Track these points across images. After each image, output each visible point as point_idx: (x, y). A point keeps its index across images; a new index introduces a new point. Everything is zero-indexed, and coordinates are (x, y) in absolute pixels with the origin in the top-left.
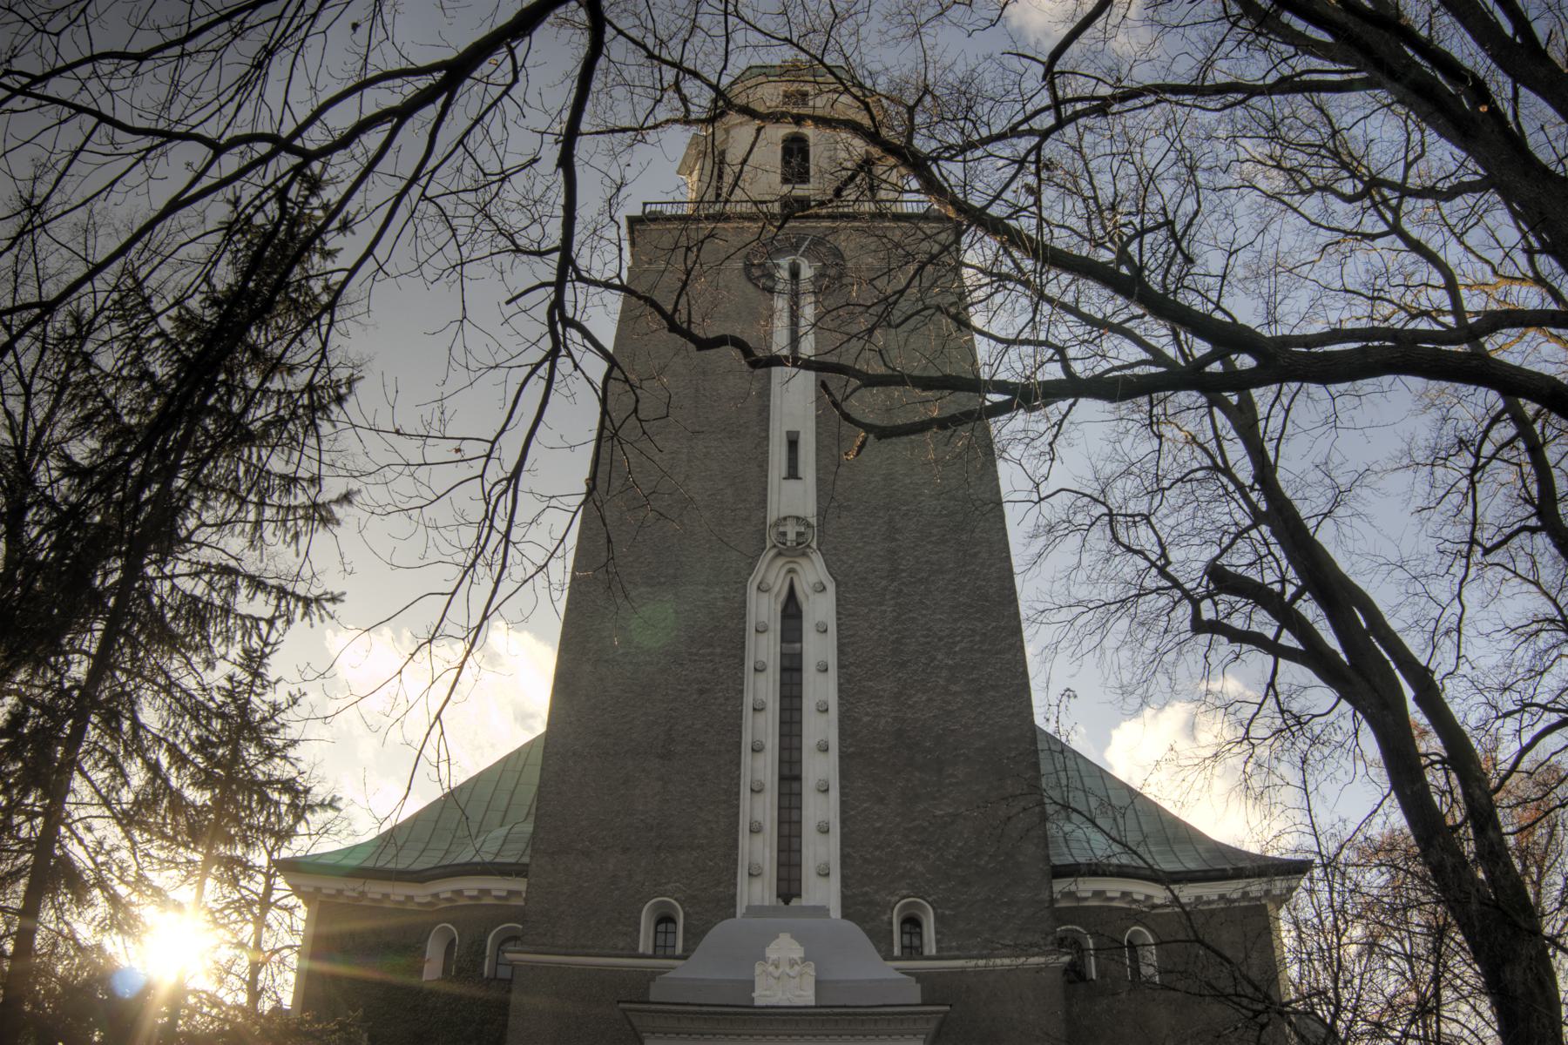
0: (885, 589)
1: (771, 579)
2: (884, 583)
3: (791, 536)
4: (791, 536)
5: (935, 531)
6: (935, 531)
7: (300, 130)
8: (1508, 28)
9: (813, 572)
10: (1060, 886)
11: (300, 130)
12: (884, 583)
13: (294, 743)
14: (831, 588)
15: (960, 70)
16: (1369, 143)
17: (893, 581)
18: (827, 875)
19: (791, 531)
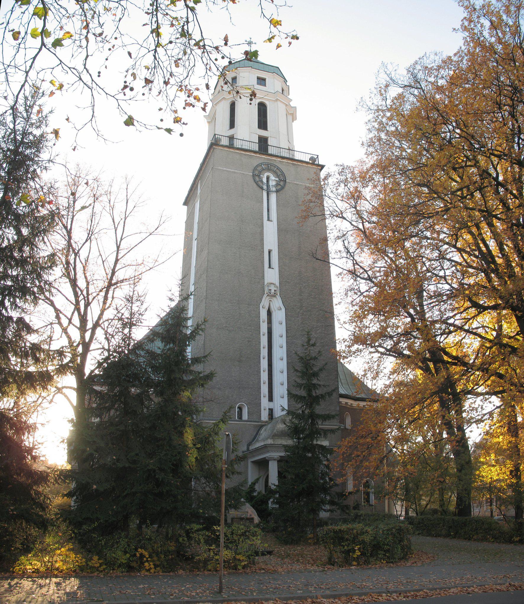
0: (299, 312)
1: (265, 304)
2: (298, 310)
3: (273, 291)
4: (273, 291)
5: (313, 294)
6: (313, 294)
7: (54, 288)
8: (484, 249)
9: (277, 303)
10: (341, 400)
11: (54, 288)
12: (298, 310)
13: (130, 296)
14: (283, 310)
15: (321, 403)
16: (469, 438)
17: (301, 310)
18: (282, 360)
19: (273, 288)
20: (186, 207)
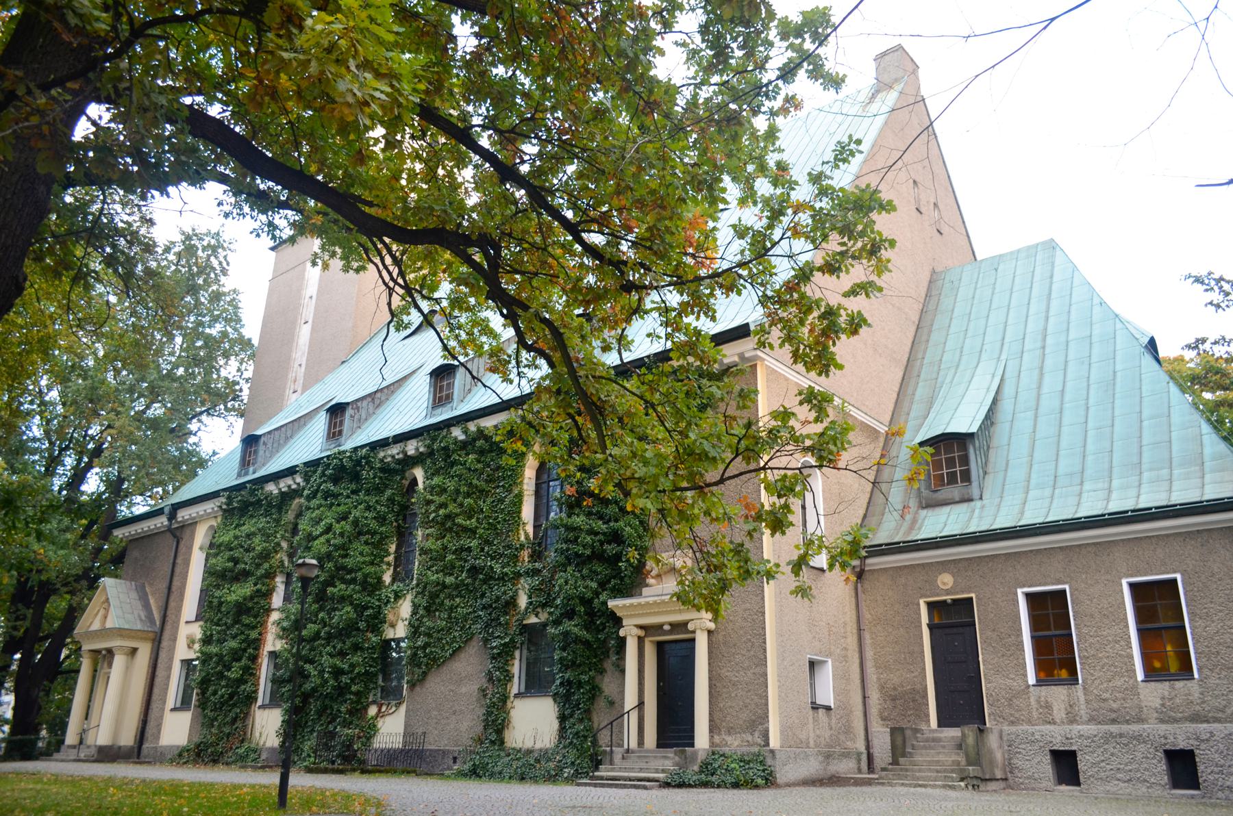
20: (273, 254)
